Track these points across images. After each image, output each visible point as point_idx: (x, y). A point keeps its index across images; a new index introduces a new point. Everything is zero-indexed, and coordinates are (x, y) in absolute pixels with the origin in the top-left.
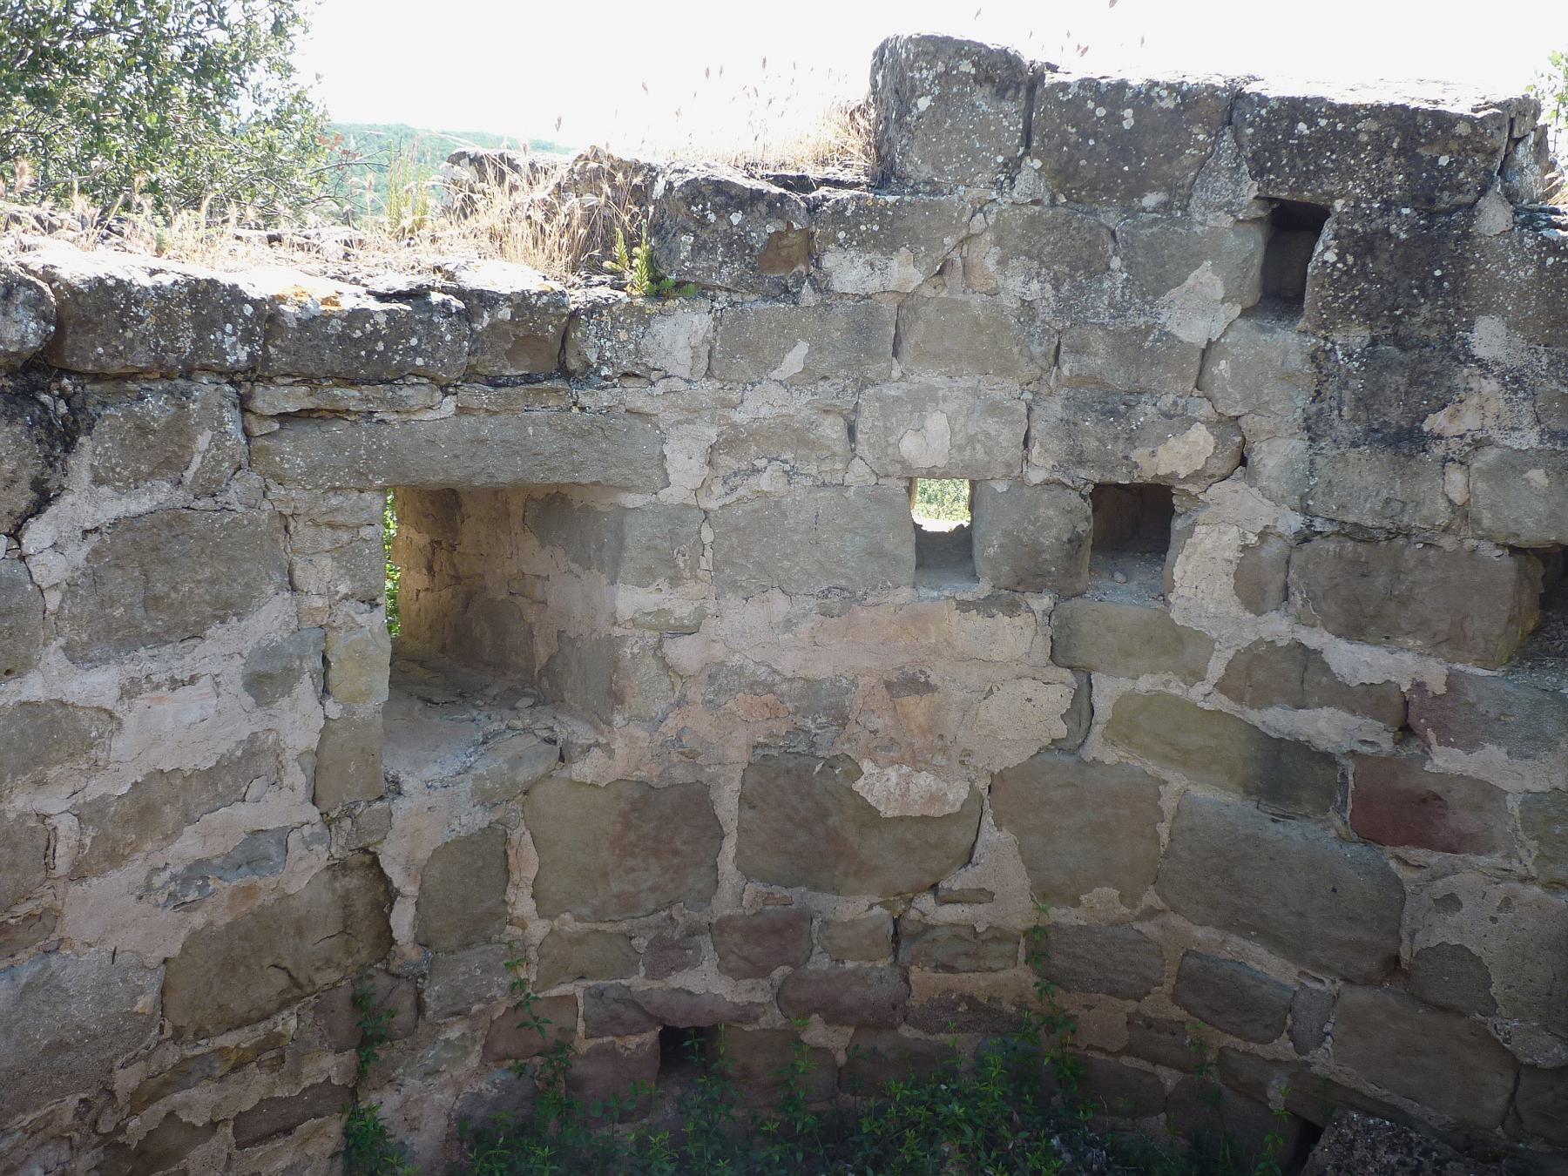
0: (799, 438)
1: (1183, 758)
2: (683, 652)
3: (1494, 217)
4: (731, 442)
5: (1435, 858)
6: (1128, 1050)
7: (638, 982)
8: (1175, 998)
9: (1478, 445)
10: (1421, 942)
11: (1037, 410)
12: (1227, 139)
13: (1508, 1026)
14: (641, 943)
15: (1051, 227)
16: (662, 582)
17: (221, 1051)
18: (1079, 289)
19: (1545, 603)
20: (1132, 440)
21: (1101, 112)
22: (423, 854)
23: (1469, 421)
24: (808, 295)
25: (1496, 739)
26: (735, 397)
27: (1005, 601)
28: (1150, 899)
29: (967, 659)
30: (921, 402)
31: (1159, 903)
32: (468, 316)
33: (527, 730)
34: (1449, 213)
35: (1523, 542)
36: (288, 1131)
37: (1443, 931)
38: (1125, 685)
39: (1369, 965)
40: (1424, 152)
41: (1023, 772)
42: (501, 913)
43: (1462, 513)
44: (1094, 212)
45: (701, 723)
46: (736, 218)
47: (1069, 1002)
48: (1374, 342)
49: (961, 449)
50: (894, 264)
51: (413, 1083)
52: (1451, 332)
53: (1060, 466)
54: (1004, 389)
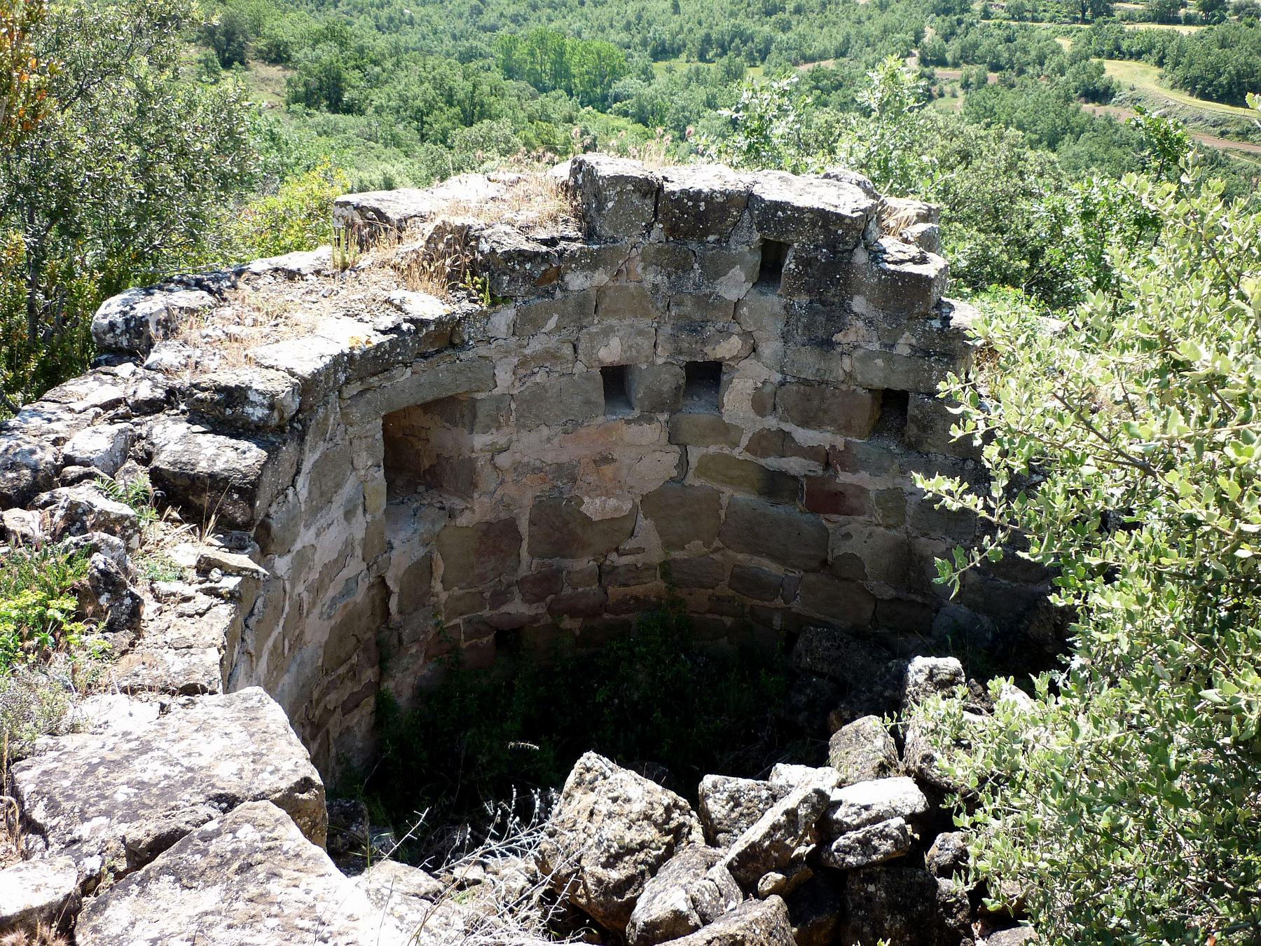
0: (552, 355)
1: (730, 481)
2: (503, 460)
3: (861, 257)
4: (523, 363)
5: (841, 518)
6: (709, 611)
7: (486, 613)
8: (730, 586)
9: (855, 347)
10: (836, 553)
11: (660, 331)
12: (747, 214)
13: (873, 584)
14: (487, 595)
15: (667, 252)
16: (493, 430)
17: (339, 676)
18: (680, 277)
19: (882, 406)
20: (704, 343)
21: (690, 204)
22: (401, 573)
23: (852, 337)
24: (558, 294)
25: (864, 469)
26: (525, 343)
27: (647, 418)
28: (717, 543)
29: (630, 445)
30: (608, 332)
31: (721, 545)
32: (416, 332)
33: (430, 505)
34: (843, 252)
35: (874, 387)
36: (357, 706)
37: (845, 548)
38: (703, 450)
39: (814, 564)
40: (832, 228)
41: (659, 493)
42: (429, 593)
43: (849, 375)
44: (686, 244)
45: (510, 490)
46: (528, 266)
47: (682, 593)
48: (811, 302)
49: (625, 352)
50: (596, 275)
51: (399, 675)
52: (844, 300)
53: (671, 356)
54: (644, 323)
